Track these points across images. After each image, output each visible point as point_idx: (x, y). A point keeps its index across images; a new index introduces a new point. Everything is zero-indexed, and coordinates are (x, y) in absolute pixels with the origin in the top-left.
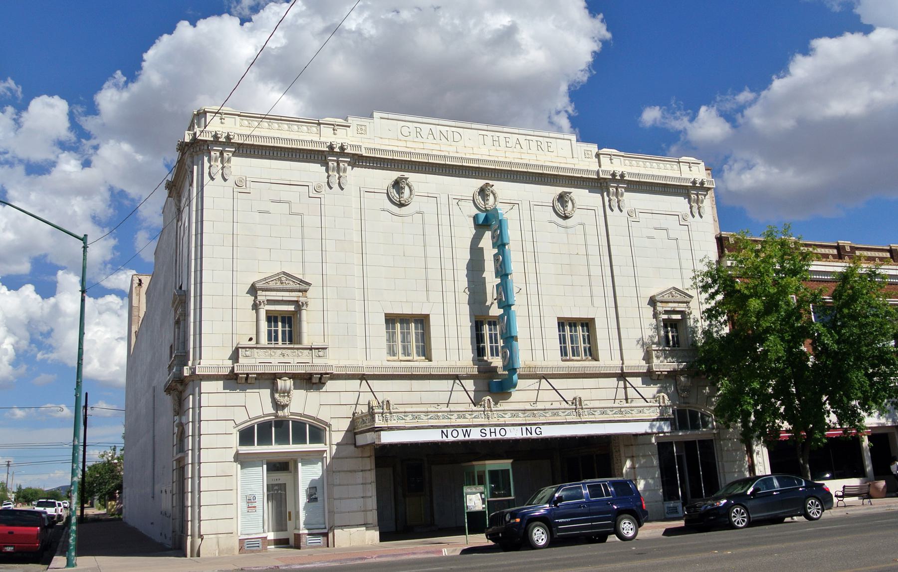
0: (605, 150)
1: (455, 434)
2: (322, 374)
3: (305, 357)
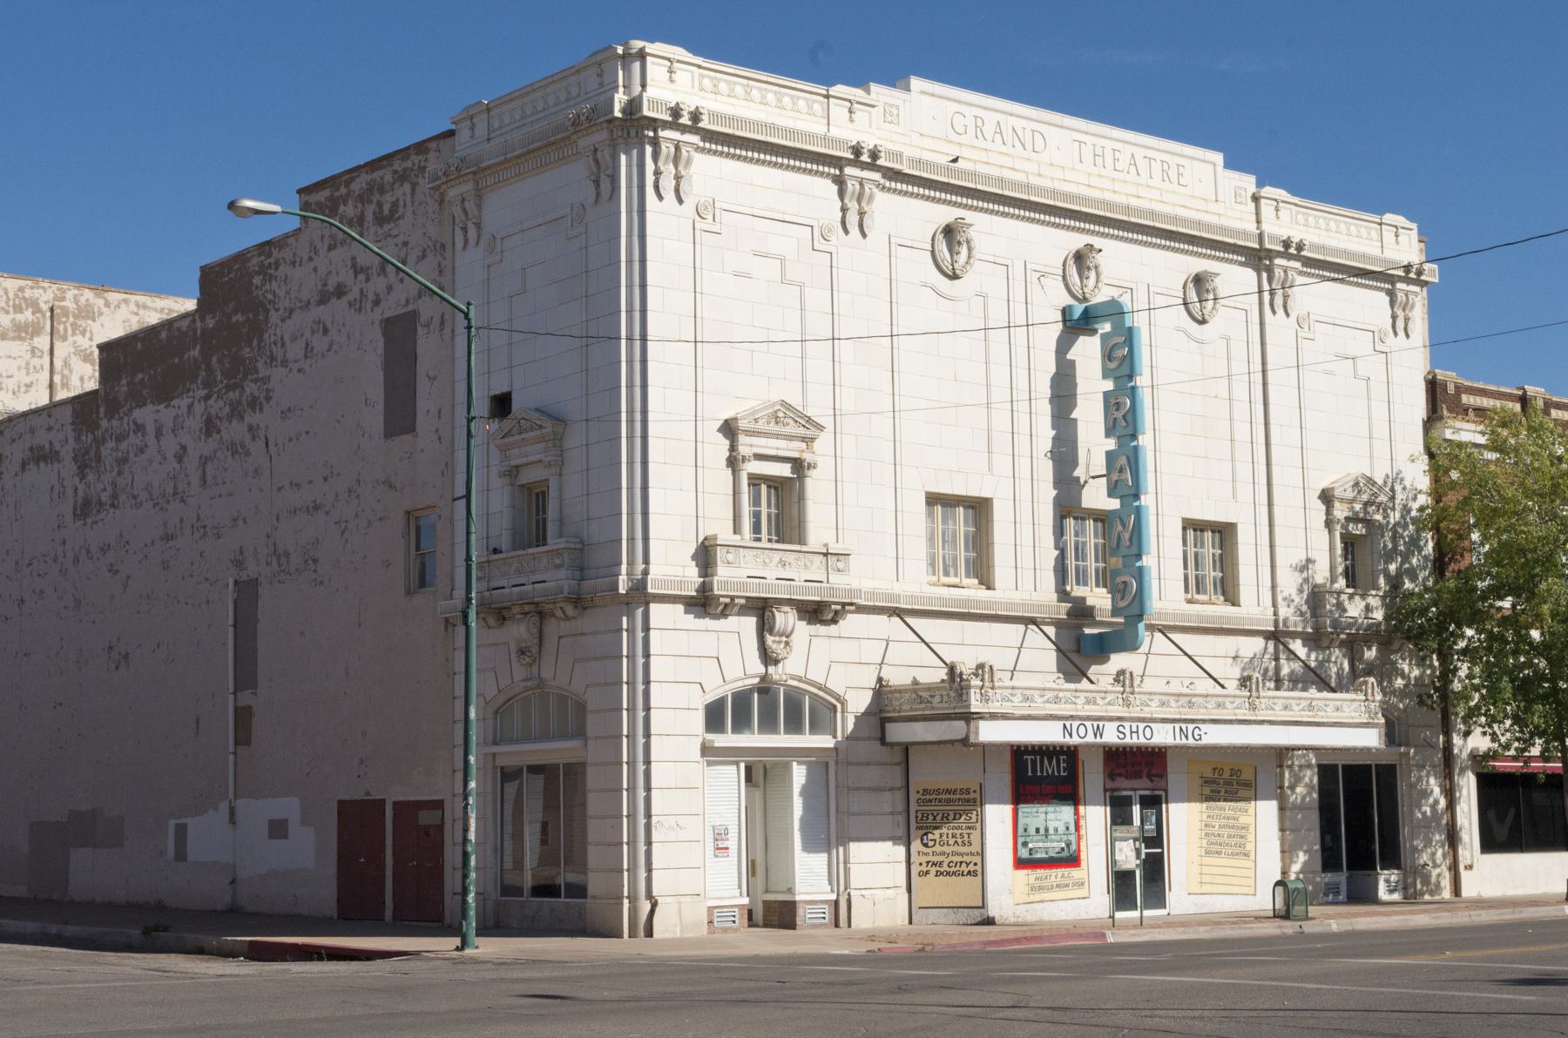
0: (1268, 191)
1: (1082, 731)
2: (844, 605)
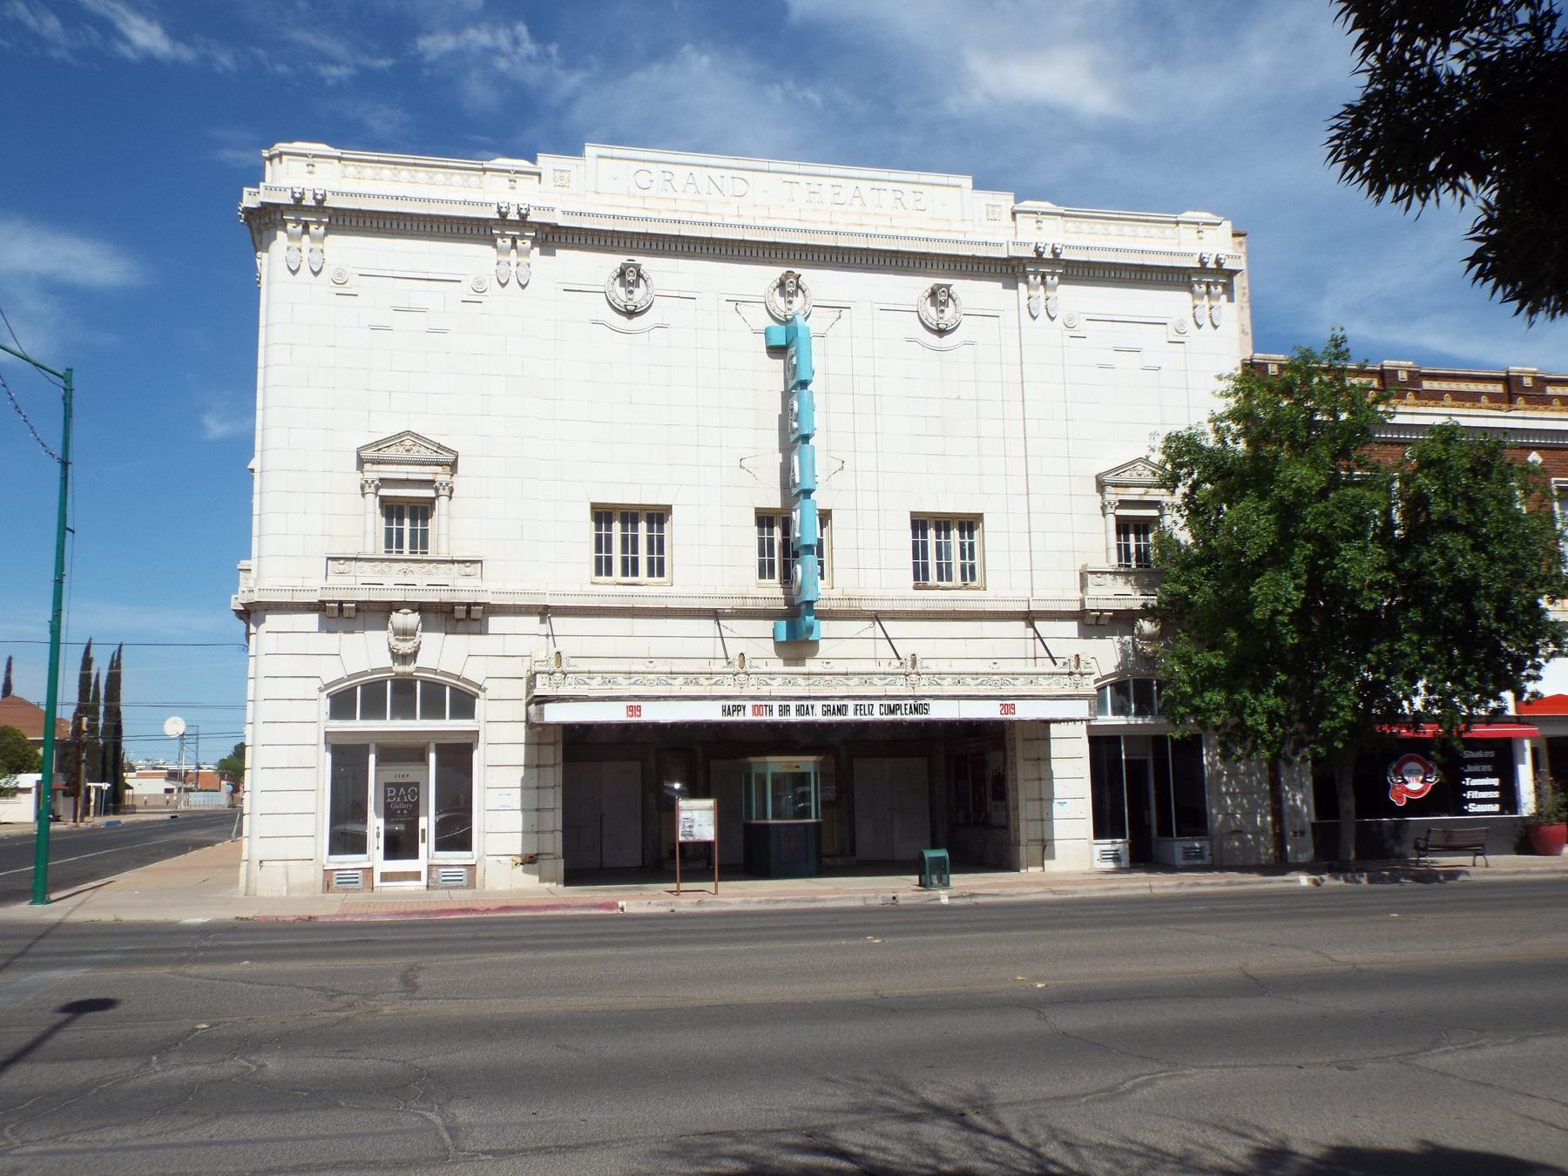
0: (1028, 205)
3: (442, 574)
